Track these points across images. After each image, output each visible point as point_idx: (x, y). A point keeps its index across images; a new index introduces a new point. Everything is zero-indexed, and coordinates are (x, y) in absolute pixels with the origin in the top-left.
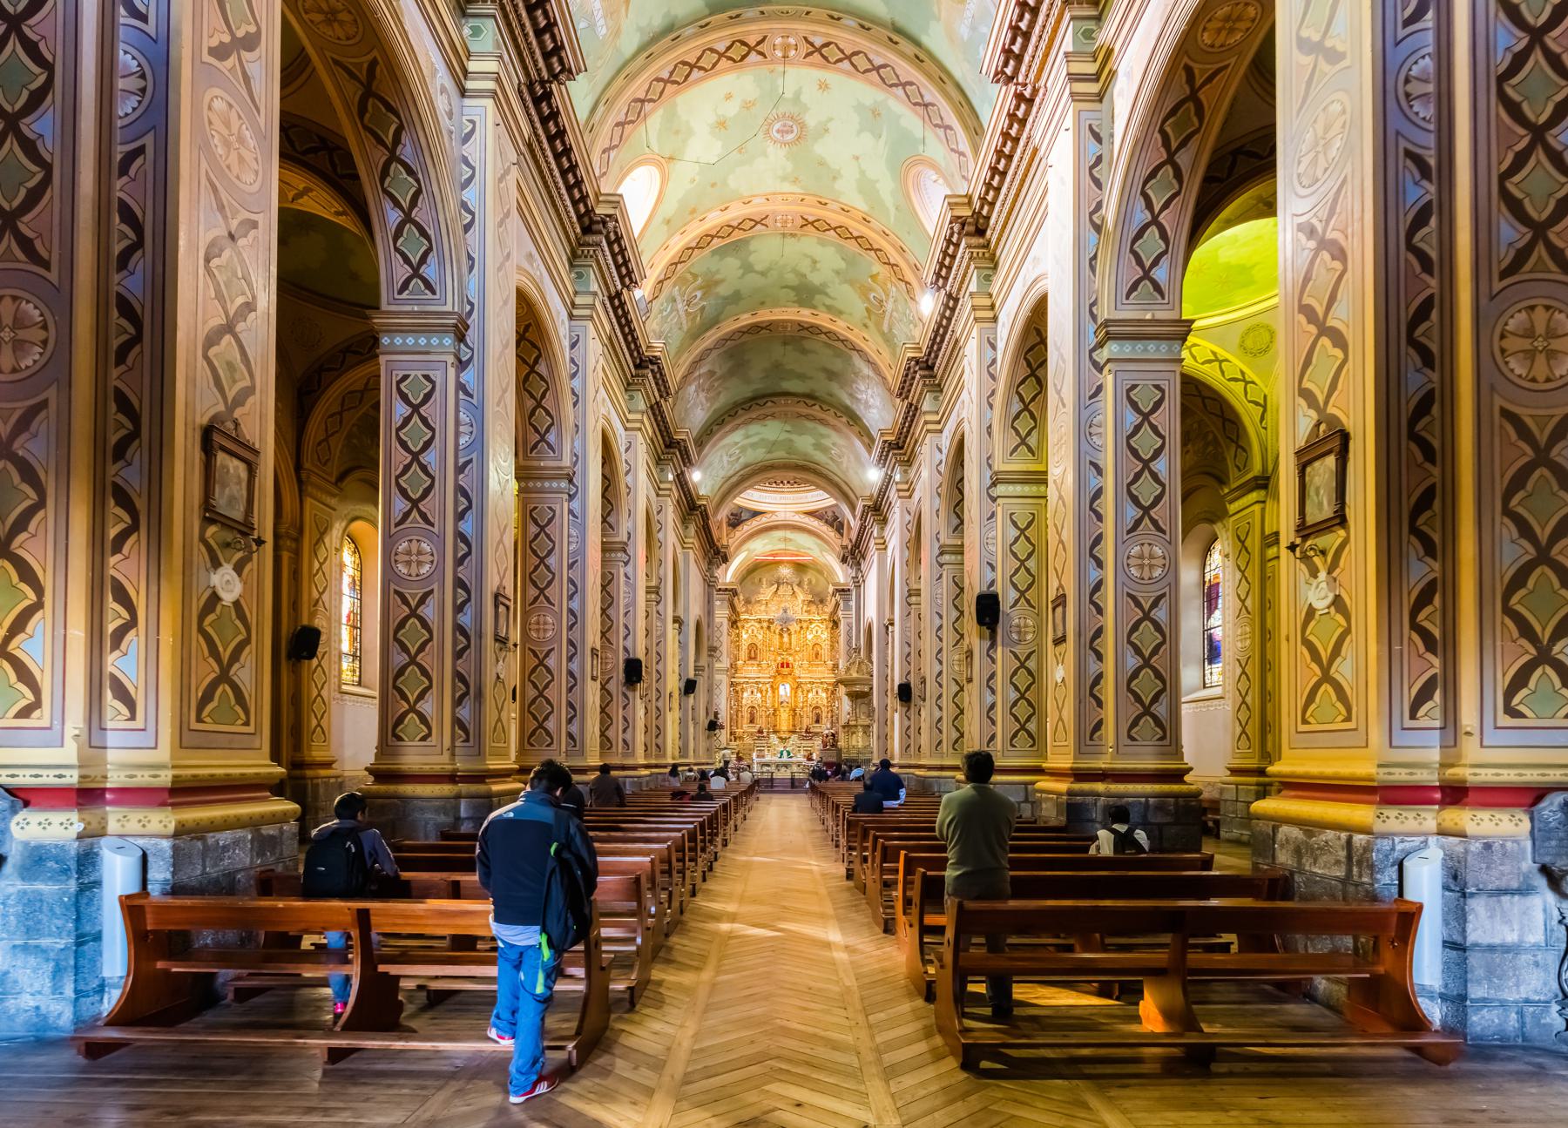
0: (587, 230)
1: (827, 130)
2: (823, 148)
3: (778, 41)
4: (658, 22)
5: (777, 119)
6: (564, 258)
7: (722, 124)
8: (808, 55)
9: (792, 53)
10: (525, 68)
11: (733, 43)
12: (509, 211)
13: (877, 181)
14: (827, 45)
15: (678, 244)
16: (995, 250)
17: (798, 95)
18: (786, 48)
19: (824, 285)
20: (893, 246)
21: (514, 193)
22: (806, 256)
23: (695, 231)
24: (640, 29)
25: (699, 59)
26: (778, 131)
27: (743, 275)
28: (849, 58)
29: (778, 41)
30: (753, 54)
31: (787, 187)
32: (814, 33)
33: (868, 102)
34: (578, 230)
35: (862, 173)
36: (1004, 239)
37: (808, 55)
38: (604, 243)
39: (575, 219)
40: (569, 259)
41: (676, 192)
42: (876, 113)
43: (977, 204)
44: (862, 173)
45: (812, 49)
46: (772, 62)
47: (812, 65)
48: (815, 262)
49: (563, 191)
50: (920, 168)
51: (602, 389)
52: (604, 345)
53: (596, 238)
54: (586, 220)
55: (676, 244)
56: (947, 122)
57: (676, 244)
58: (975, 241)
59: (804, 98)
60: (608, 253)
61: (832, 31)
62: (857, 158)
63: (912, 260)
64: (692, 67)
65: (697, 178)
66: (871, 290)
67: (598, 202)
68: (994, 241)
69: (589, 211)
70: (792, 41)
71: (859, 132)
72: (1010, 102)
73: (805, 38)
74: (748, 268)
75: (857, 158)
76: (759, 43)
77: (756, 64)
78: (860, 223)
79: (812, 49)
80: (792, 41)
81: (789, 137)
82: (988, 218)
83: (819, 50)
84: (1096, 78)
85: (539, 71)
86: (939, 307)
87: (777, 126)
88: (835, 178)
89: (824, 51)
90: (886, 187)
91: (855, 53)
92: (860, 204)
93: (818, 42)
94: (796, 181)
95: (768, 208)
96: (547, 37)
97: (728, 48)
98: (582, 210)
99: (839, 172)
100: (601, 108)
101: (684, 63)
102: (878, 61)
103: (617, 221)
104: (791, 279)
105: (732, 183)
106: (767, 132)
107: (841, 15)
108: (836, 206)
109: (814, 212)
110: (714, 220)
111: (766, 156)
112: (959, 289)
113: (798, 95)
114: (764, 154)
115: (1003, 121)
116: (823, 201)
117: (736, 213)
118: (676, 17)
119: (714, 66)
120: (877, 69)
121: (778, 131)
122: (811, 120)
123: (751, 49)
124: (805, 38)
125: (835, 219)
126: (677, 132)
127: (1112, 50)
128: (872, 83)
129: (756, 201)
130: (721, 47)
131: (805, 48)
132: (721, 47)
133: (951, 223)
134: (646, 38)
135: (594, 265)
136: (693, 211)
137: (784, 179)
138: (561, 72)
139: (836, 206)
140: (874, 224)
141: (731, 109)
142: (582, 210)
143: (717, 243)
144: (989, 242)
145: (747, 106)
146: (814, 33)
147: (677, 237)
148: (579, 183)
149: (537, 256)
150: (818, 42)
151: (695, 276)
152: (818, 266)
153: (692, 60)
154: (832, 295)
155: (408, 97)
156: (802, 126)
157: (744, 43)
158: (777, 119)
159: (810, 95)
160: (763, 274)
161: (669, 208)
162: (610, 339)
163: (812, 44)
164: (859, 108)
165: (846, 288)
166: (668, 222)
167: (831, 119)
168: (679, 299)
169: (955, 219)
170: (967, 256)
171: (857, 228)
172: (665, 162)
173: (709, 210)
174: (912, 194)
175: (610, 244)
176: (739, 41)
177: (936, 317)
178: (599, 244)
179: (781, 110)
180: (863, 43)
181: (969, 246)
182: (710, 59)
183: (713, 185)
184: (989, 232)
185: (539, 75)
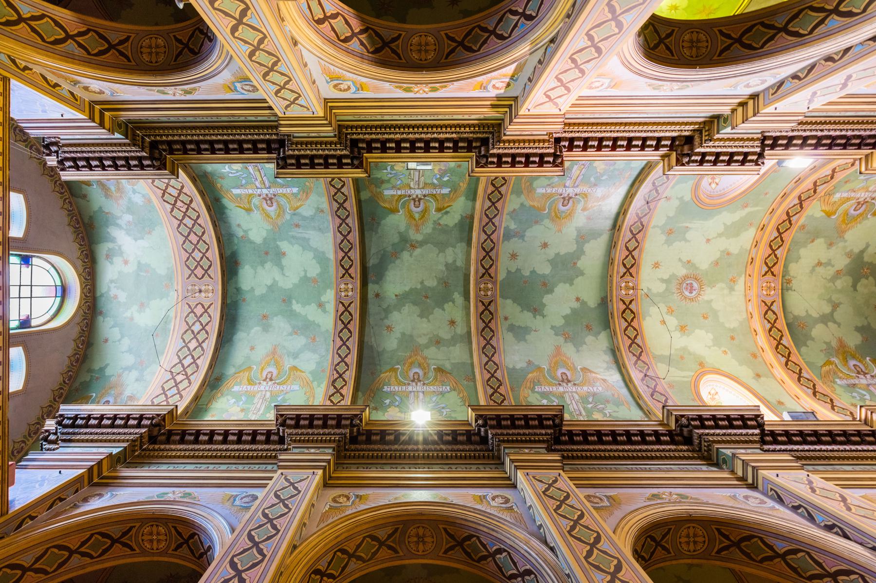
0: (688, 441)
1: (689, 262)
2: (703, 263)
3: (623, 292)
4: (608, 358)
5: (682, 293)
6: (704, 468)
7: (683, 328)
8: (631, 275)
9: (631, 284)
10: (539, 441)
11: (623, 317)
12: (841, 496)
13: (725, 224)
14: (624, 265)
15: (780, 372)
16: (700, 123)
17: (663, 281)
18: (627, 288)
19: (849, 254)
20: (781, 203)
21: (830, 485)
22: (813, 270)
23: (770, 355)
24: (608, 369)
25: (629, 337)
26: (691, 293)
27: (835, 322)
28: (631, 252)
29: (623, 292)
30: (630, 306)
31: (740, 286)
32: (618, 272)
33: (663, 238)
34: (685, 448)
35: (720, 235)
36: (685, 120)
37: (631, 275)
38: (701, 431)
39: (673, 447)
40: (708, 465)
41: (730, 364)
42: (670, 232)
43: (663, 151)
44: (720, 235)
45: (628, 273)
46: (636, 296)
47: (637, 273)
48: (820, 264)
49: (645, 447)
50: (702, 197)
51: (846, 492)
52: (802, 468)
53: (695, 437)
54: (275, 438)
55: (780, 374)
56: (650, 186)
57: (780, 374)
58: (697, 141)
59: (666, 277)
60: (712, 431)
61: (616, 263)
62: (708, 241)
63: (792, 185)
64: (633, 342)
65: (723, 349)
66: (846, 213)
67: (668, 425)
68: (691, 127)
69: (670, 433)
70: (623, 285)
71: (686, 241)
72: (576, 152)
73: (621, 277)
74: (826, 319)
75: (708, 241)
76: (624, 303)
77: (637, 305)
78: (764, 233)
79: (628, 273)
80: (623, 285)
81: (695, 285)
82: (673, 139)
83: (628, 270)
84: (332, 108)
85: (546, 434)
86: (792, 150)
87: (687, 293)
88: (728, 254)
89: (628, 266)
90: (727, 218)
91: (627, 249)
92: (750, 234)
93: (624, 270)
94: (733, 281)
95: (755, 300)
96: (531, 423)
97: (626, 320)
98: (667, 438)
99: (722, 252)
100: (641, 402)
101: (630, 346)
102: (629, 235)
103: (682, 416)
104: (844, 282)
105: (734, 325)
106: (692, 300)
107: (750, 258)
108: (754, 251)
109: (759, 267)
110: (762, 340)
111: (712, 300)
112: (752, 139)
113: (663, 281)
114: (710, 302)
115: (634, 152)
116: (750, 260)
117: (758, 324)
118: (607, 347)
119: (635, 329)
120: (634, 236)
121: (691, 293)
122: (682, 272)
123: (628, 308)
124: (621, 277)
125: (763, 251)
126: (682, 358)
127: (491, 105)
128: (644, 237)
129: (750, 309)
130: (625, 324)
131: (628, 277)
132: (625, 324)
133: (683, 165)
134: (614, 366)
135: (717, 446)
136: (754, 356)
137: (732, 289)
138: (553, 421)
139: (754, 251)
140: (765, 221)
141: (672, 322)
142: (667, 438)
143: (787, 341)
144: (694, 130)
145: (670, 311)
146: (618, 272)
147: (775, 372)
148: (642, 433)
149: (188, 490)
150: (624, 270)
151: (828, 363)
152: (823, 261)
153: (630, 341)
154: (862, 247)
155: (463, 522)
156: (686, 277)
157: (624, 312)
158: (682, 293)
159: (664, 273)
160: (835, 306)
161: (745, 373)
162: (799, 458)
163: (625, 274)
164: (668, 243)
165: (848, 236)
166: (758, 376)
167: (680, 260)
168: (852, 381)
169: (679, 162)
170: (711, 144)
171: (770, 233)
172: (703, 369)
173: (755, 342)
174: (728, 198)
175: (703, 426)
176: (622, 314)
177: (808, 150)
178: (700, 436)
179: (674, 290)
180: (621, 245)
181: (701, 145)
182: (631, 333)
183: (733, 338)
184: (687, 133)
185: (548, 435)
